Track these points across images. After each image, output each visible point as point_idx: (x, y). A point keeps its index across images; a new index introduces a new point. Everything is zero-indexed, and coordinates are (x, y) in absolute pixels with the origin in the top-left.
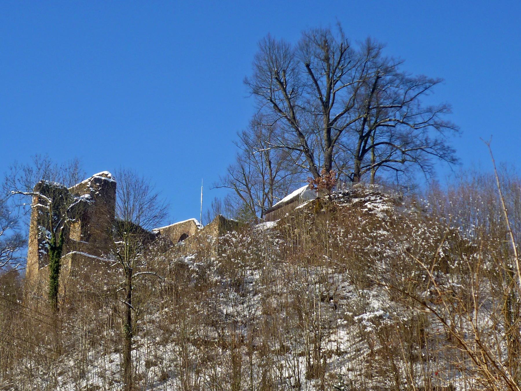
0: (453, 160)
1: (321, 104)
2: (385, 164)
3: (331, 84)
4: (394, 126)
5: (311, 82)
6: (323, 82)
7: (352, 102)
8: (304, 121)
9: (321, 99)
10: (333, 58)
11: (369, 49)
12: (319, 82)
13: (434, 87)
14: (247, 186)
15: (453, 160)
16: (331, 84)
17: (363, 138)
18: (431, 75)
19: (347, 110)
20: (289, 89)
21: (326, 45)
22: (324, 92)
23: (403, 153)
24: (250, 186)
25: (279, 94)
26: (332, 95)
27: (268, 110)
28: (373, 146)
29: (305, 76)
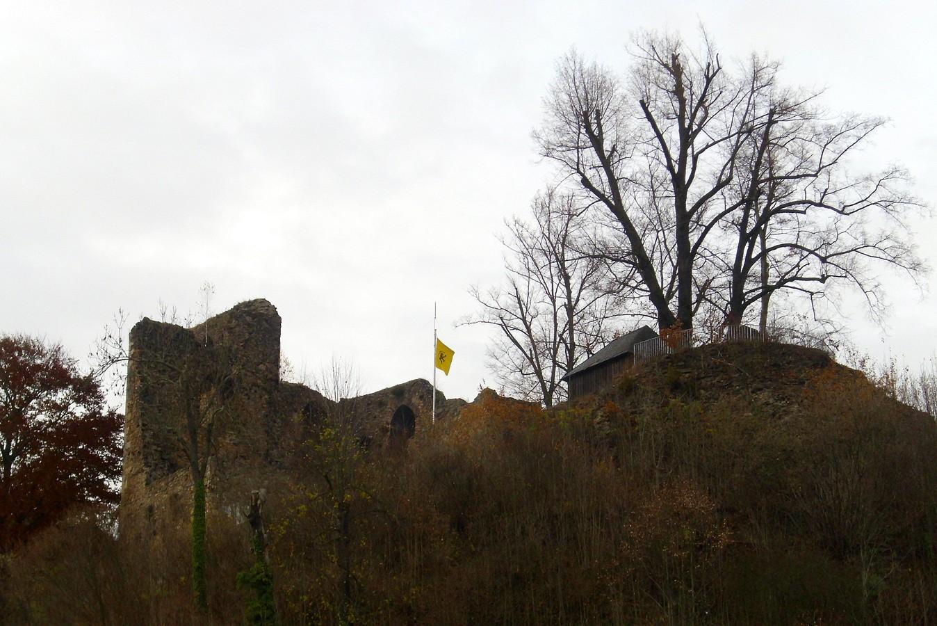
0: (915, 266)
1: (670, 177)
2: (789, 284)
3: (687, 137)
4: (804, 212)
5: (652, 133)
6: (673, 136)
7: (727, 172)
8: (635, 202)
9: (670, 167)
10: (683, 92)
11: (757, 80)
12: (665, 137)
13: (872, 136)
14: (524, 320)
15: (915, 266)
16: (687, 137)
17: (746, 238)
18: (866, 111)
19: (720, 185)
20: (607, 146)
21: (676, 70)
22: (675, 155)
23: (824, 260)
24: (528, 319)
25: (590, 155)
26: (689, 160)
27: (572, 184)
28: (765, 252)
29: (637, 122)
